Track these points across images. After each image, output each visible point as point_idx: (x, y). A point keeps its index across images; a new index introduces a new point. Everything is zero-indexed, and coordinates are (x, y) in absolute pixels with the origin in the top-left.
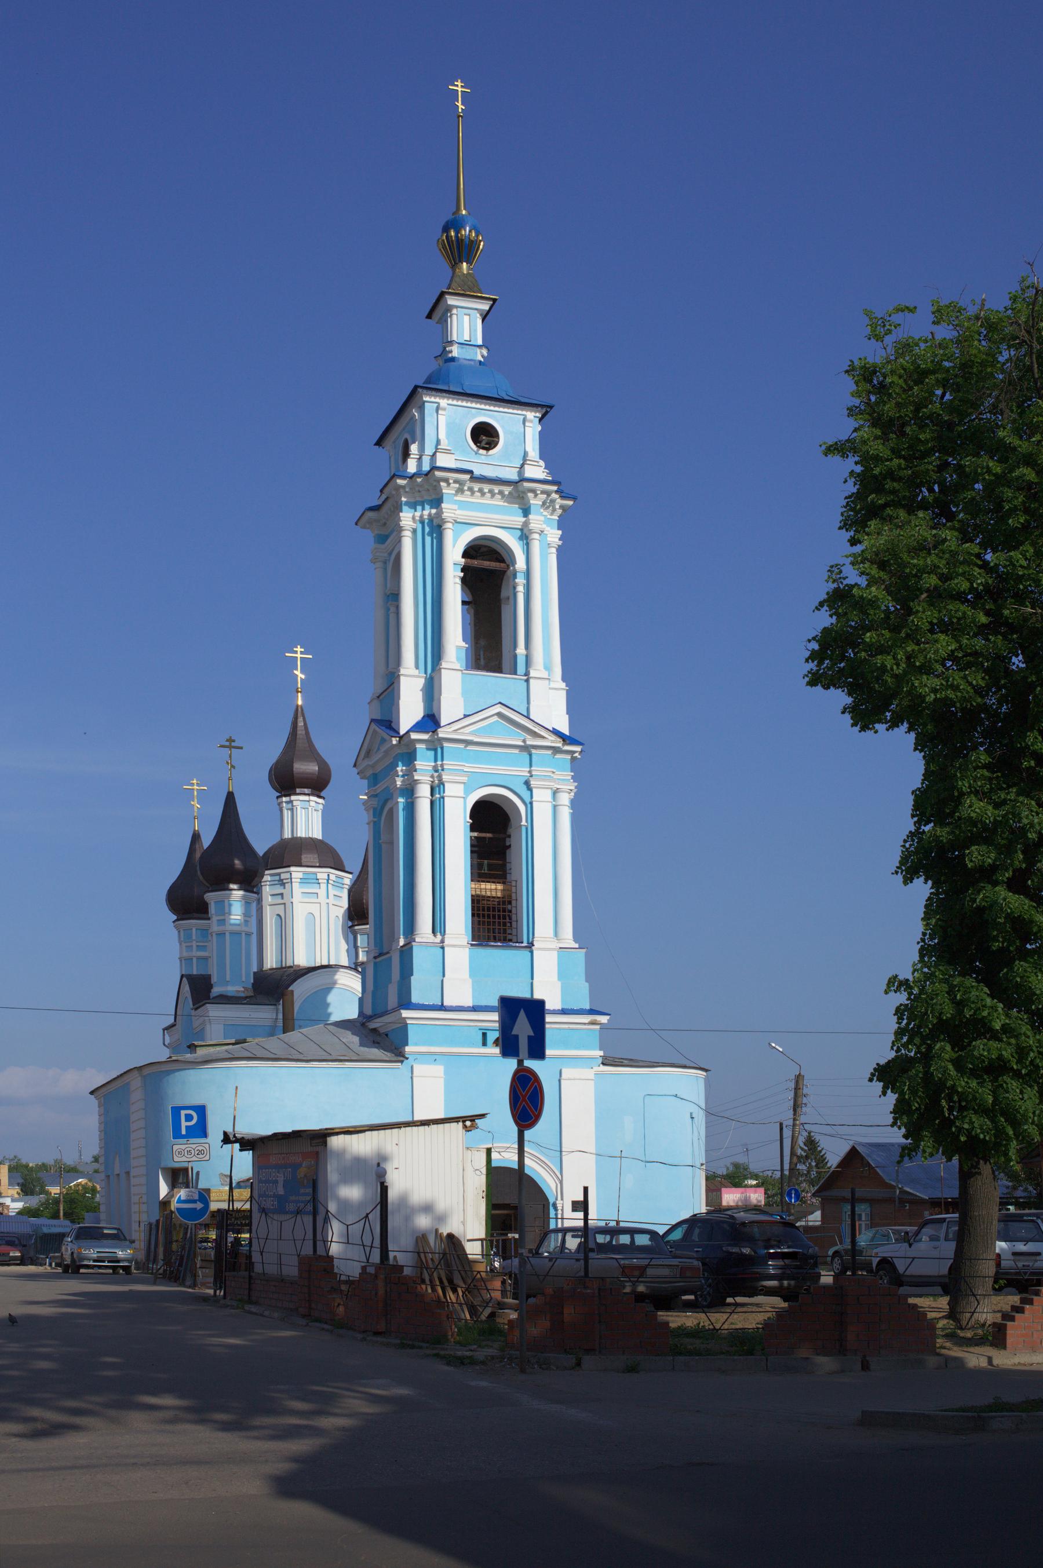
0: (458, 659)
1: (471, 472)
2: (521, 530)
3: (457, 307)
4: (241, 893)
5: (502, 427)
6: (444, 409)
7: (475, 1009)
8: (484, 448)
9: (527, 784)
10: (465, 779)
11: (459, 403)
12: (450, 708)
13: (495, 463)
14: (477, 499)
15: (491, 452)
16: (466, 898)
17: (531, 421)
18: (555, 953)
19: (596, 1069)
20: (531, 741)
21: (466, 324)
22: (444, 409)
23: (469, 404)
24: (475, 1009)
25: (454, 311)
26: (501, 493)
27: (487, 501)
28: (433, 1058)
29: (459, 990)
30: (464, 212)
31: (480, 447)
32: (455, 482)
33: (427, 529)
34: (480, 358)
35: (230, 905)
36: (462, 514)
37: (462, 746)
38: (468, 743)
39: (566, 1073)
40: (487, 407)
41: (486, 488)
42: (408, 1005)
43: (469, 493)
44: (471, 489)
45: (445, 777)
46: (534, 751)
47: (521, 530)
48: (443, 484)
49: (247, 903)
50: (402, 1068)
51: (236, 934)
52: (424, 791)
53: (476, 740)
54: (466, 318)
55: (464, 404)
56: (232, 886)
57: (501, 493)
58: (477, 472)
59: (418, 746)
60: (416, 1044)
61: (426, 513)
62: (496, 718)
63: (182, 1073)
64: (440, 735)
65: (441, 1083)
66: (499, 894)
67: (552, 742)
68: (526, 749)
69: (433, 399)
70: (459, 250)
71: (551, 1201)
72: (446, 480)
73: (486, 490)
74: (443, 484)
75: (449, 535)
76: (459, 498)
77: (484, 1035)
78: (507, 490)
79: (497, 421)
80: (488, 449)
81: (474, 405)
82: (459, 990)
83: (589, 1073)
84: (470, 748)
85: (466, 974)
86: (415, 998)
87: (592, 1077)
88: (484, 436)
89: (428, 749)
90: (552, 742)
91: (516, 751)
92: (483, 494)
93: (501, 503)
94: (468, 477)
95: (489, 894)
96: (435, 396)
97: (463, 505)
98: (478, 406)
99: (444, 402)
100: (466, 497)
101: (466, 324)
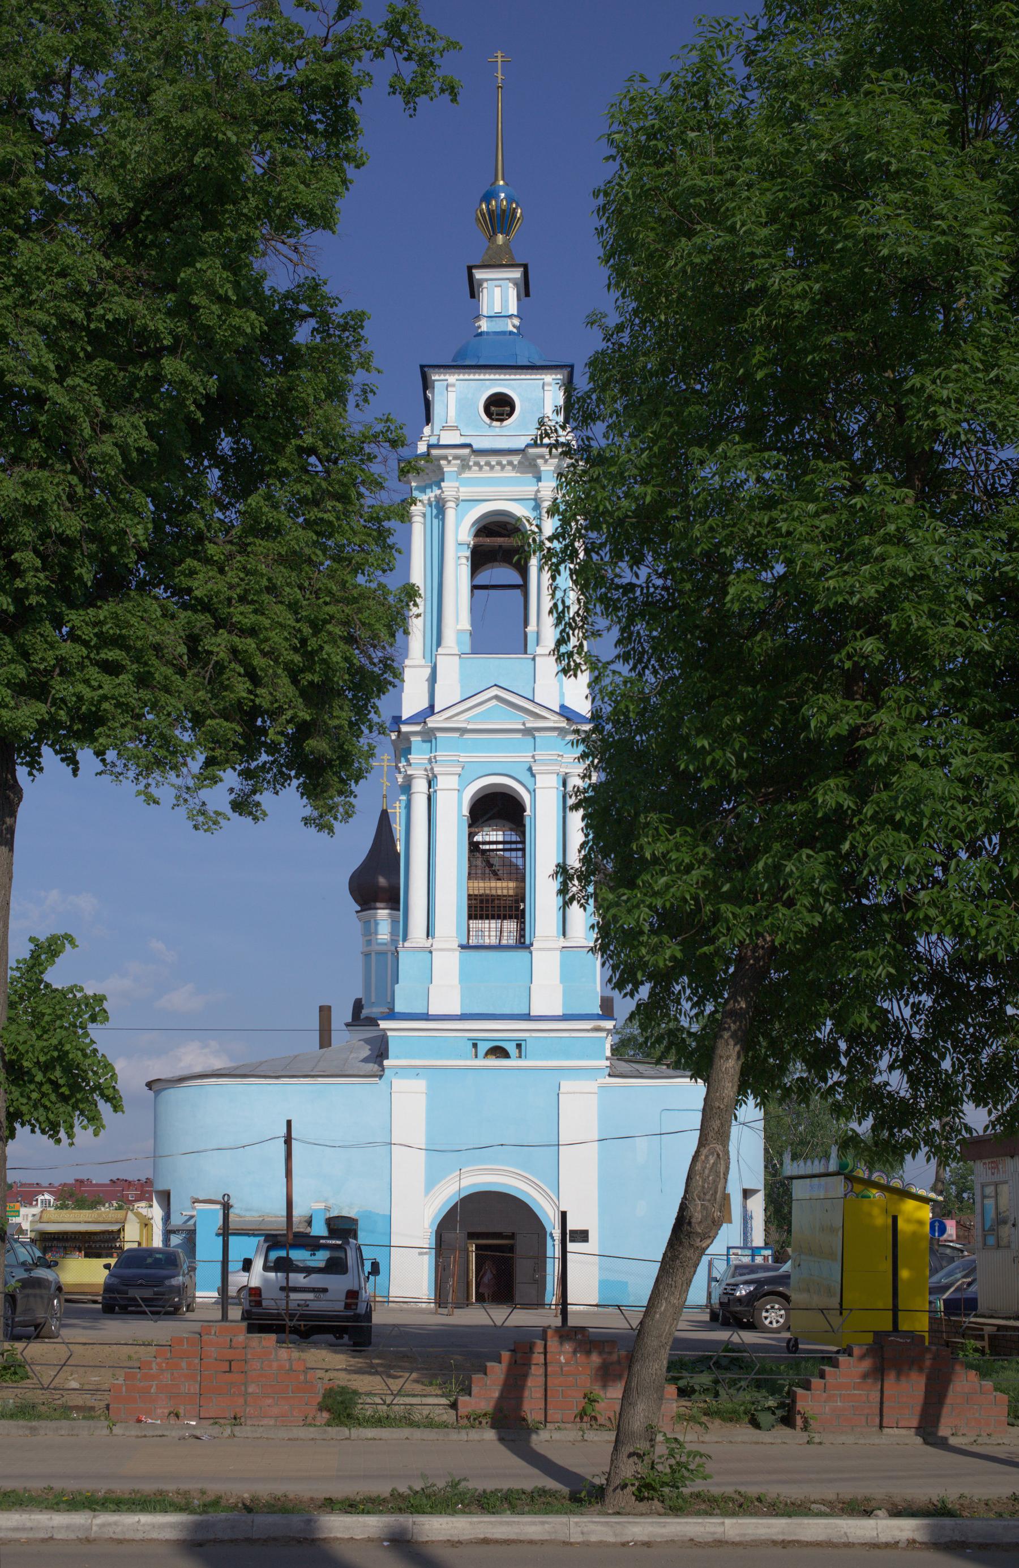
0: (459, 643)
1: (469, 446)
2: (535, 499)
3: (487, 280)
4: (387, 911)
5: (519, 395)
6: (453, 385)
7: (565, 1018)
8: (497, 420)
9: (530, 769)
10: (459, 770)
11: (472, 377)
12: (447, 694)
13: (516, 432)
14: (486, 473)
15: (505, 423)
16: (459, 898)
17: (550, 384)
18: (557, 954)
19: (600, 1081)
20: (532, 723)
21: (499, 296)
22: (453, 385)
23: (482, 377)
24: (565, 1018)
25: (485, 285)
26: (510, 463)
27: (497, 474)
28: (416, 1071)
29: (446, 995)
30: (501, 183)
31: (492, 419)
32: (456, 458)
33: (435, 512)
34: (511, 328)
35: (377, 924)
36: (465, 492)
37: (456, 735)
38: (463, 731)
39: (566, 1086)
40: (502, 377)
41: (493, 460)
42: (392, 1015)
43: (476, 468)
44: (477, 464)
45: (436, 770)
46: (537, 734)
47: (535, 499)
48: (443, 462)
49: (395, 922)
50: (382, 1083)
51: (381, 954)
52: (420, 786)
53: (469, 727)
54: (497, 291)
55: (477, 377)
56: (379, 905)
57: (510, 463)
58: (475, 446)
59: (413, 739)
60: (397, 1057)
61: (432, 495)
62: (494, 702)
63: (172, 1090)
64: (430, 725)
65: (422, 1100)
66: (511, 892)
67: (555, 722)
68: (528, 732)
69: (442, 377)
70: (500, 221)
71: (548, 1230)
72: (445, 458)
73: (493, 463)
74: (443, 462)
75: (450, 514)
76: (466, 475)
77: (475, 1045)
78: (516, 459)
79: (513, 389)
80: (502, 420)
81: (487, 377)
82: (446, 995)
83: (592, 1086)
84: (467, 736)
85: (455, 981)
86: (399, 1008)
87: (596, 1090)
88: (499, 407)
89: (424, 741)
90: (555, 722)
91: (519, 736)
92: (492, 467)
93: (513, 474)
94: (467, 451)
95: (499, 892)
96: (440, 374)
97: (470, 482)
98: (492, 377)
99: (452, 378)
100: (473, 474)
101: (499, 296)
